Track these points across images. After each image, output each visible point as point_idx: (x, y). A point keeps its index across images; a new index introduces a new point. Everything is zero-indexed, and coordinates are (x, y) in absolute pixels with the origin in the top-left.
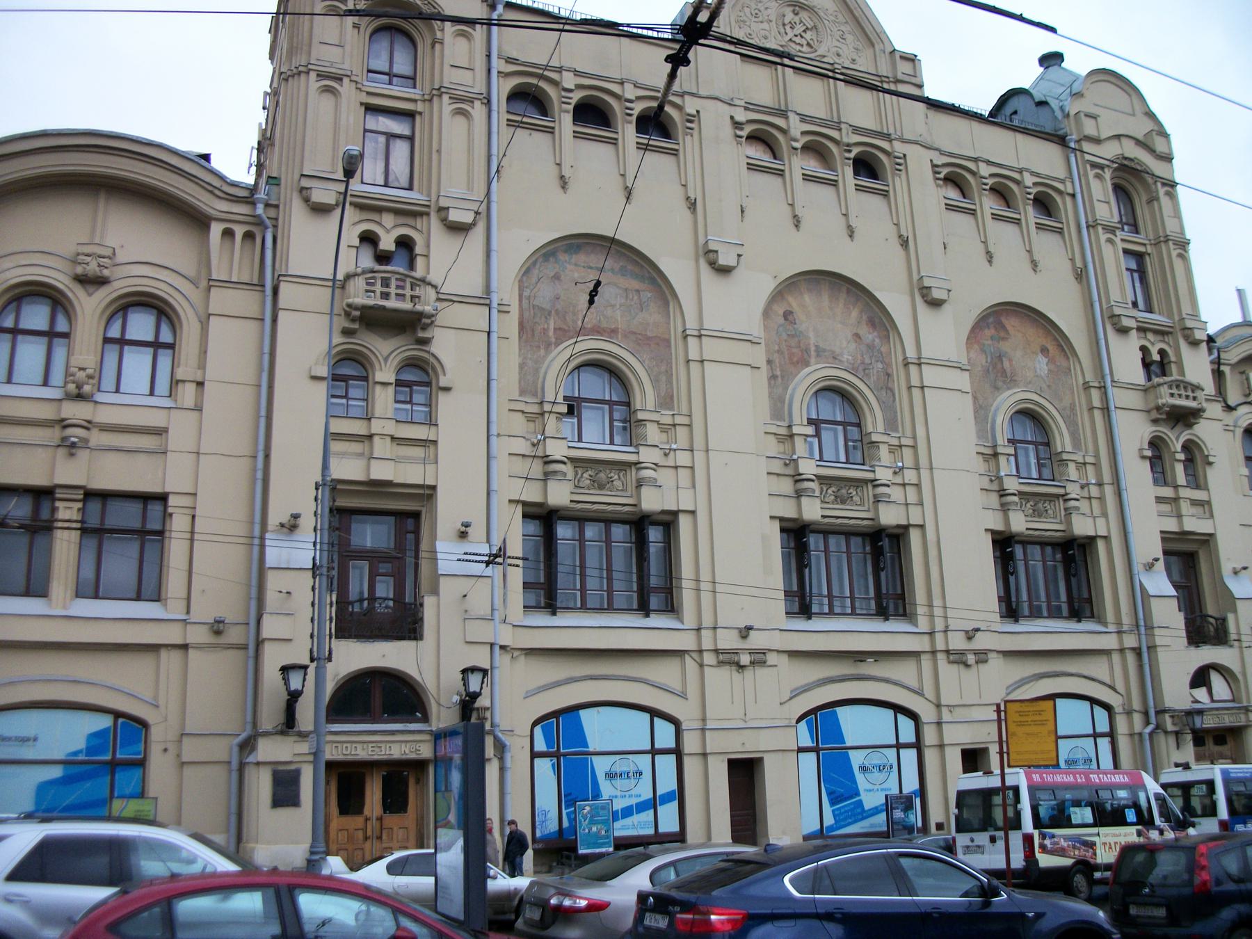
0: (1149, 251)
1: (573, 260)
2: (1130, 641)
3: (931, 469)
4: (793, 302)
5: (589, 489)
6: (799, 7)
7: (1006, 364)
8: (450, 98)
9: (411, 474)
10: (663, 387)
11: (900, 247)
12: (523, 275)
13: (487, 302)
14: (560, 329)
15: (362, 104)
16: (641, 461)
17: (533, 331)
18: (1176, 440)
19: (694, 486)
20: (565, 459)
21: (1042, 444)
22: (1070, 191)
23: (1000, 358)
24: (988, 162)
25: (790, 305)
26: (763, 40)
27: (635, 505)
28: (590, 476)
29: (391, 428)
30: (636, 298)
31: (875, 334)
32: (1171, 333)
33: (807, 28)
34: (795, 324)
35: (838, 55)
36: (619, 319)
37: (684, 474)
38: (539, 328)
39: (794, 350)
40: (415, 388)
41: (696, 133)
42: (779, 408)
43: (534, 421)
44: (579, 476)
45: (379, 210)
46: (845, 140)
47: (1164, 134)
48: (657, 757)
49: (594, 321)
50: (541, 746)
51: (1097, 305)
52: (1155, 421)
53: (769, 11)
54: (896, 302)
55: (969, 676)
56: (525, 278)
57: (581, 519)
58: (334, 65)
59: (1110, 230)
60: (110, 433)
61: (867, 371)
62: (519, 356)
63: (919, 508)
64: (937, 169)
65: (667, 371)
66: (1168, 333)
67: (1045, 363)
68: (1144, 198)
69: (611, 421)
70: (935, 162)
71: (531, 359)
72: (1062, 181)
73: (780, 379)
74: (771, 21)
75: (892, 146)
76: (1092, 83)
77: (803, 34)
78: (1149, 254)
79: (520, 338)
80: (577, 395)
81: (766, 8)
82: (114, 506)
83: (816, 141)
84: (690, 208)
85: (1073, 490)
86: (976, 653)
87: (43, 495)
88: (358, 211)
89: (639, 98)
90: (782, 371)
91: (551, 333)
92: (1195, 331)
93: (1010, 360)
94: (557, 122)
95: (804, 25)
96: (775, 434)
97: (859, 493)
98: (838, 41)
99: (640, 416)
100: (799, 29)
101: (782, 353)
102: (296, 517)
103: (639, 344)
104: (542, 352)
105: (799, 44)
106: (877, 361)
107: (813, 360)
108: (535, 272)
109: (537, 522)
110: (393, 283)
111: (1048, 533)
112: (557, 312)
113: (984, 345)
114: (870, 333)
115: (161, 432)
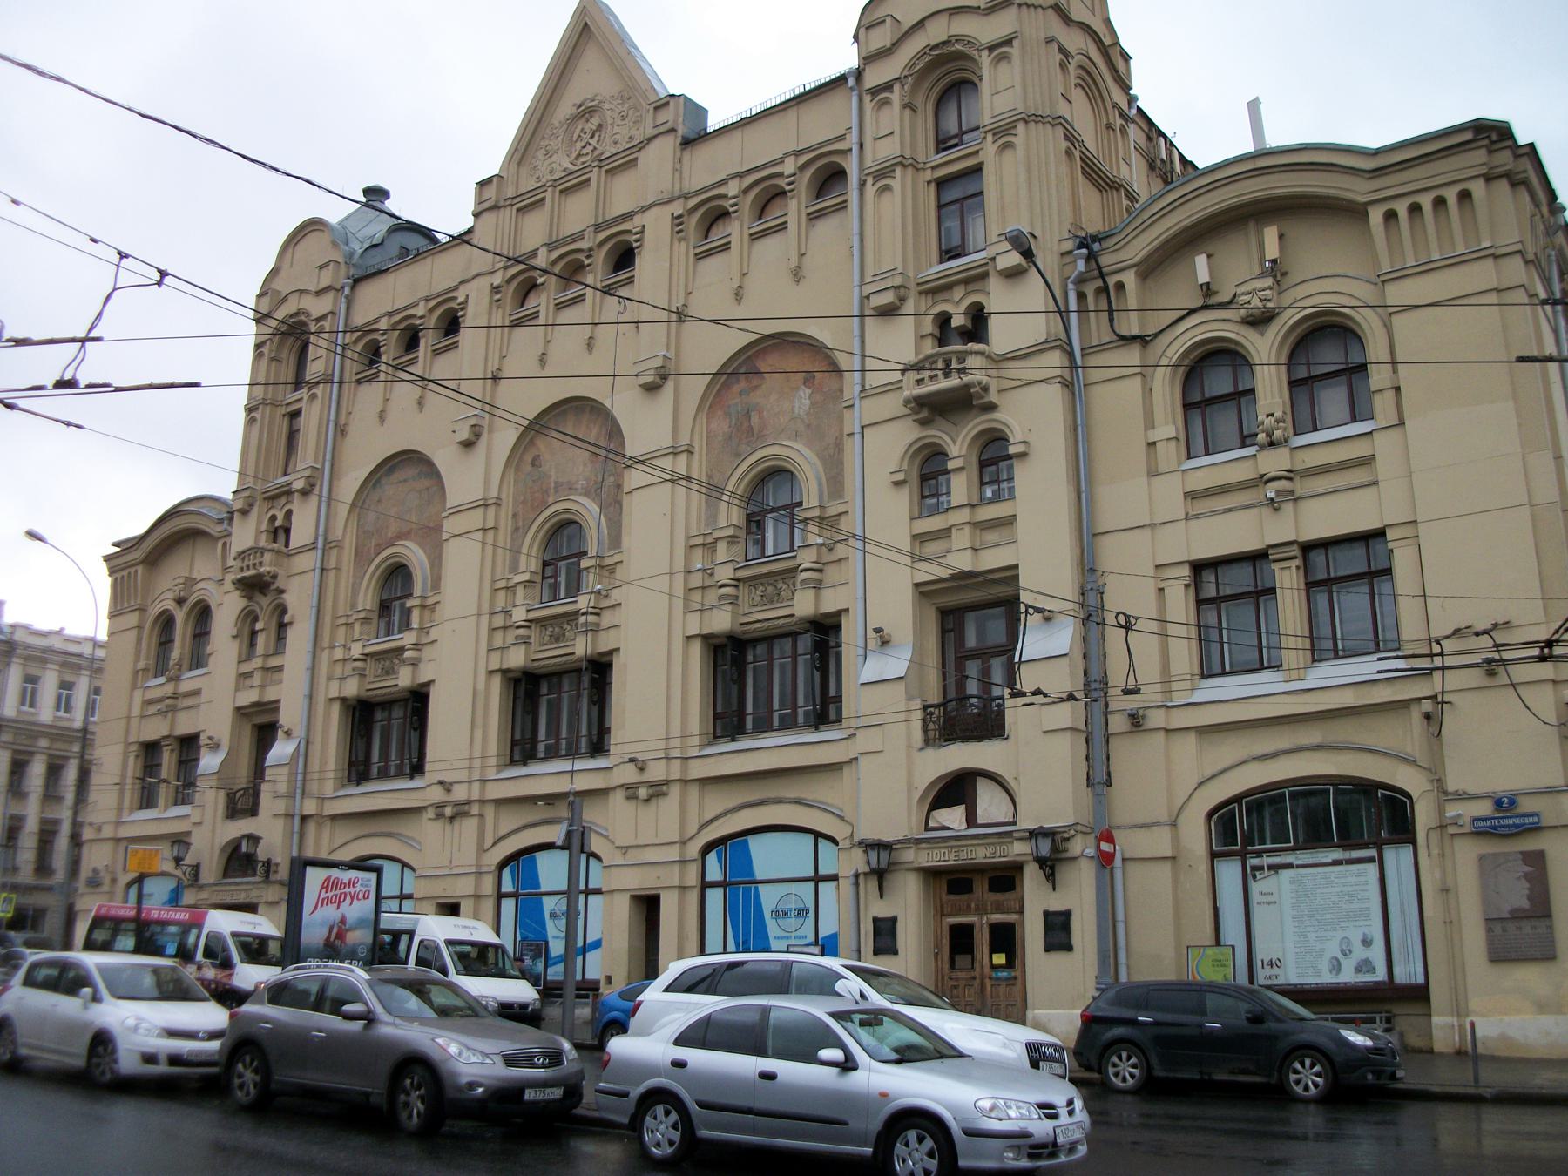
4: (542, 444)
7: (755, 419)
18: (958, 444)
23: (748, 415)
39: (537, 495)
45: (949, 287)
48: (821, 885)
50: (508, 886)
55: (647, 814)
60: (1338, 472)
67: (807, 396)
79: (355, 561)
82: (1337, 553)
83: (615, 244)
87: (1257, 558)
111: (781, 622)
115: (1368, 461)
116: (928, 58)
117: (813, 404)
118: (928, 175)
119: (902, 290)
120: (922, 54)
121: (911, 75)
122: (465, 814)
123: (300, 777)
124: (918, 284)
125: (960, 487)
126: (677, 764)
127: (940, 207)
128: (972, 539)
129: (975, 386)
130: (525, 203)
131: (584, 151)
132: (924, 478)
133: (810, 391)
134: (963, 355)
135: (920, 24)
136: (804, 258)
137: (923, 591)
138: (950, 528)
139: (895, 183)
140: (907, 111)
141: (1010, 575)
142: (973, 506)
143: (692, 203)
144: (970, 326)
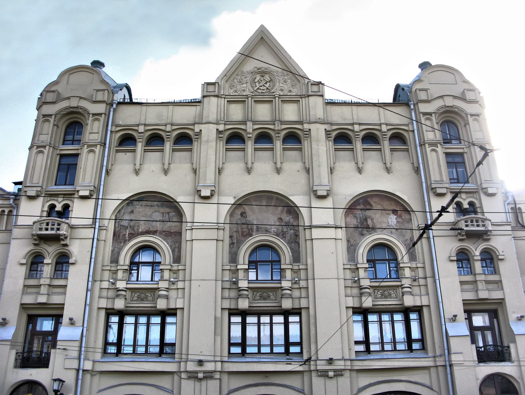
0: (465, 151)
1: (140, 204)
2: (440, 362)
3: (314, 279)
5: (380, 298)
6: (263, 73)
7: (369, 222)
8: (428, 145)
9: (496, 295)
10: (176, 253)
11: (415, 173)
12: (118, 213)
13: (94, 226)
14: (131, 234)
15: (444, 153)
16: (159, 287)
17: (119, 236)
19: (184, 298)
20: (369, 287)
21: (488, 259)
22: (411, 129)
23: (366, 220)
24: (360, 124)
25: (245, 210)
26: (243, 92)
27: (402, 304)
28: (381, 293)
29: (483, 277)
30: (167, 216)
31: (291, 217)
32: (477, 192)
33: (267, 82)
34: (247, 217)
35: (282, 90)
36: (158, 226)
37: (423, 289)
38: (121, 235)
39: (245, 230)
40: (463, 261)
41: (309, 140)
42: (233, 259)
43: (355, 272)
44: (132, 296)
46: (276, 128)
47: (473, 90)
49: (147, 228)
51: (424, 185)
52: (460, 240)
53: (247, 78)
54: (299, 200)
55: (331, 384)
56: (118, 214)
57: (379, 312)
58: (44, 142)
59: (433, 144)
61: (284, 235)
62: (112, 247)
63: (307, 299)
64: (328, 133)
65: (178, 246)
66: (475, 192)
67: (395, 218)
68: (463, 124)
69: (389, 267)
70: (327, 129)
71: (117, 248)
72: (407, 125)
73: (236, 244)
74: (247, 83)
75: (303, 127)
76: (428, 74)
77: (265, 85)
78: (466, 153)
80: (387, 258)
81: (246, 78)
84: (415, 173)
85: (406, 282)
86: (335, 371)
88: (452, 194)
89: (388, 130)
90: (237, 240)
91: (127, 236)
92: (488, 189)
93: (372, 220)
94: (303, 146)
95: (266, 80)
96: (350, 269)
97: (274, 294)
98: (283, 84)
99: (401, 265)
100: (263, 83)
101: (238, 232)
102: (455, 316)
103: (166, 236)
104: (122, 244)
105: (263, 89)
106: (291, 230)
107: (254, 233)
108: (123, 211)
109: (402, 313)
110: (475, 221)
112: (130, 226)
113: (356, 214)
114: (287, 217)
116: (68, 111)
117: (397, 222)
118: (58, 152)
119: (92, 192)
120: (66, 108)
121: (438, 113)
122: (211, 378)
123: (83, 349)
124: (46, 191)
125: (47, 270)
126: (219, 364)
127: (60, 164)
128: (48, 291)
129: (62, 236)
130: (290, 99)
131: (262, 88)
132: (32, 264)
133: (396, 217)
134: (484, 220)
135: (69, 98)
136: (113, 166)
137: (24, 307)
138: (41, 285)
139: (46, 151)
140: (56, 127)
141: (61, 307)
142: (51, 278)
143: (335, 127)
144: (62, 212)
